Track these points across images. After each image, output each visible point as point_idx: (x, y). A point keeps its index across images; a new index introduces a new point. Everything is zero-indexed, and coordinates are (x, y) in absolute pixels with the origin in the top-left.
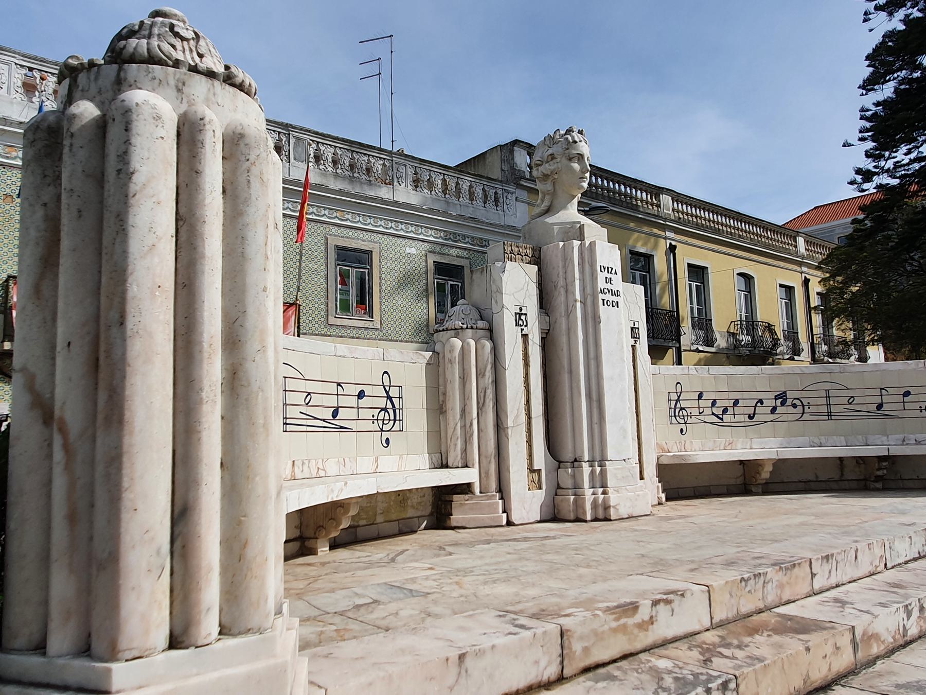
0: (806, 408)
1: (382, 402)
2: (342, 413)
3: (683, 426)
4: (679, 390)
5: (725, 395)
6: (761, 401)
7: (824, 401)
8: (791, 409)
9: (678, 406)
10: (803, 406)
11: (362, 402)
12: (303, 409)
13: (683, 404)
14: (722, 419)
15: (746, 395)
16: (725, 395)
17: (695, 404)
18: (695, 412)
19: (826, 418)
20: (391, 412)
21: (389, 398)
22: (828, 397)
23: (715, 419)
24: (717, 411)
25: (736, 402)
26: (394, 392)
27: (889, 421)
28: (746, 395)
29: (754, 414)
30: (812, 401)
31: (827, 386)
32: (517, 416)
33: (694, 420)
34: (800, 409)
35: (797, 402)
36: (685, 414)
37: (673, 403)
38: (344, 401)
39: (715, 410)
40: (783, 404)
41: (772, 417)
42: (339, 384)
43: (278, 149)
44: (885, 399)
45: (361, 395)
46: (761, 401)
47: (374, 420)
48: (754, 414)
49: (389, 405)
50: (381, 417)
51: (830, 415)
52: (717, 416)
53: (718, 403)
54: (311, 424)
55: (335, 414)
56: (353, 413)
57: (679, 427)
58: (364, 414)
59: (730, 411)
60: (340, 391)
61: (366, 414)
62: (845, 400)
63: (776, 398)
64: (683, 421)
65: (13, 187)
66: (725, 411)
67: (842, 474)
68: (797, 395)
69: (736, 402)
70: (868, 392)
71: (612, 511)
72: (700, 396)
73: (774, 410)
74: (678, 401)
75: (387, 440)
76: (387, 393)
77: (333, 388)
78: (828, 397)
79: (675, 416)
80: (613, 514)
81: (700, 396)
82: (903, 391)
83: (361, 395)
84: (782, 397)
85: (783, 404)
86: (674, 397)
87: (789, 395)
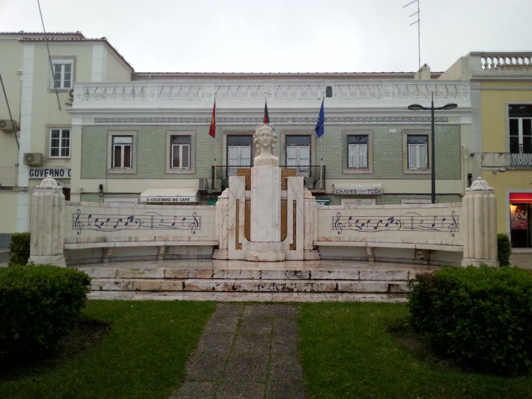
1: (452, 222)
2: (436, 226)
3: (340, 231)
5: (103, 217)
6: (381, 221)
7: (150, 221)
8: (395, 225)
9: (78, 221)
10: (401, 223)
11: (444, 222)
13: (80, 220)
15: (374, 218)
16: (103, 217)
18: (86, 224)
21: (454, 220)
25: (369, 221)
26: (456, 218)
27: (176, 230)
28: (374, 218)
30: (145, 221)
31: (412, 215)
32: (232, 226)
33: (85, 228)
34: (139, 224)
35: (398, 222)
37: (75, 219)
38: (176, 221)
39: (358, 224)
40: (391, 222)
41: (125, 227)
43: (414, 107)
45: (444, 220)
46: (381, 221)
47: (448, 228)
49: (195, 222)
51: (412, 228)
52: (358, 227)
54: (423, 228)
55: (433, 225)
56: (440, 226)
57: (77, 231)
59: (366, 225)
61: (446, 226)
62: (419, 222)
63: (128, 218)
66: (363, 225)
67: (213, 254)
68: (138, 217)
69: (369, 221)
70: (429, 218)
72: (90, 216)
73: (387, 225)
74: (338, 220)
75: (454, 235)
77: (433, 218)
81: (90, 216)
82: (443, 218)
83: (444, 220)
85: (391, 222)
86: (76, 216)
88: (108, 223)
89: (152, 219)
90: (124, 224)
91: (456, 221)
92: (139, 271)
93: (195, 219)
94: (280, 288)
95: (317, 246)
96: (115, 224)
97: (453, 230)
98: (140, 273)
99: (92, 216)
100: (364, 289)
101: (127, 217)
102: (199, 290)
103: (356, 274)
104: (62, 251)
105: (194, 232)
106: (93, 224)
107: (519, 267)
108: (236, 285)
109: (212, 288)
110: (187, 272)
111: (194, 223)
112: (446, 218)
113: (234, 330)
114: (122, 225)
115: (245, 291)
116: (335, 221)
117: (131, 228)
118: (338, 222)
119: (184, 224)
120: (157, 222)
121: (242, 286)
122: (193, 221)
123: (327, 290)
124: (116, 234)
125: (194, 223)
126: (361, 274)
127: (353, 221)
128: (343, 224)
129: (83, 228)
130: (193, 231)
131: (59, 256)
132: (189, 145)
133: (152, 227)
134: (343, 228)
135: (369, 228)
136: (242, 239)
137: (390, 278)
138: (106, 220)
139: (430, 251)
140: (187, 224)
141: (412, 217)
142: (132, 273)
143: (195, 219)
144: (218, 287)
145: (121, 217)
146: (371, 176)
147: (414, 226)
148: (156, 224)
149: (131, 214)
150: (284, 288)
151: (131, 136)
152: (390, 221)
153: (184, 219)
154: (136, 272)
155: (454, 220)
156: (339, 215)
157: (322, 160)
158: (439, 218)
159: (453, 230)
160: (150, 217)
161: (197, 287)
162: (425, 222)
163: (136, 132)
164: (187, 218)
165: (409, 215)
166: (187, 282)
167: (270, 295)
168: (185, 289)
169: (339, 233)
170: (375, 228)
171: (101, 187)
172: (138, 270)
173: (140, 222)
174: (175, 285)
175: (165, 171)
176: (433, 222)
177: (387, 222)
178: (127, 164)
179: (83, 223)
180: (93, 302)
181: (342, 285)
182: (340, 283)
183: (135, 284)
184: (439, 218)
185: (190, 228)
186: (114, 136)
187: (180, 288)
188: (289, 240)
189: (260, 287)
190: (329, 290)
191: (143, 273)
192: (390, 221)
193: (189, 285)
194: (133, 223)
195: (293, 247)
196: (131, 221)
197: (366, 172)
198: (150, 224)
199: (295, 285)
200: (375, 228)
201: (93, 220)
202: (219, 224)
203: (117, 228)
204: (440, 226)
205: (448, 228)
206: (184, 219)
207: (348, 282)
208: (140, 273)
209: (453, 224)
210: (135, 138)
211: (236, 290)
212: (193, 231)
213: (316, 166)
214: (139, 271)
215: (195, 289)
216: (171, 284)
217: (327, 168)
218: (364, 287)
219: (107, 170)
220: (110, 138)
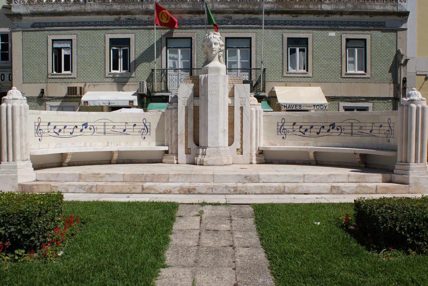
0: (343, 130)
1: (387, 128)
2: (373, 131)
3: (284, 136)
4: (39, 121)
6: (76, 127)
8: (336, 131)
9: (39, 128)
11: (381, 128)
13: (41, 127)
14: (58, 134)
17: (46, 127)
18: (46, 131)
19: (350, 135)
20: (146, 130)
21: (390, 127)
23: (301, 134)
24: (57, 131)
25: (65, 127)
26: (391, 125)
27: (128, 136)
29: (320, 132)
30: (98, 127)
31: (352, 121)
32: (182, 132)
33: (45, 134)
34: (93, 130)
35: (338, 127)
36: (42, 132)
38: (127, 127)
39: (301, 130)
40: (86, 128)
42: (373, 123)
44: (374, 128)
46: (76, 127)
47: (385, 134)
48: (320, 132)
49: (390, 129)
50: (387, 133)
52: (56, 133)
53: (57, 127)
55: (371, 131)
56: (378, 132)
57: (282, 136)
58: (381, 132)
59: (62, 131)
60: (373, 125)
61: (383, 132)
62: (358, 128)
63: (83, 125)
64: (40, 135)
65: (269, 32)
69: (65, 127)
71: (204, 162)
72: (49, 124)
73: (81, 130)
74: (39, 126)
76: (389, 125)
77: (371, 124)
78: (352, 126)
79: (280, 132)
80: (204, 163)
81: (49, 124)
82: (380, 124)
83: (381, 126)
84: (85, 125)
85: (333, 128)
86: (37, 124)
87: (336, 124)
88: (65, 130)
89: (105, 126)
90: (326, 131)
91: (392, 128)
92: (100, 176)
93: (145, 125)
94: (232, 190)
96: (71, 131)
97: (388, 136)
99: (51, 124)
100: (309, 191)
101: (82, 124)
102: (157, 192)
103: (301, 177)
104: (29, 158)
105: (144, 138)
108: (191, 188)
110: (144, 176)
111: (144, 129)
112: (383, 125)
113: (197, 227)
114: (77, 130)
115: (199, 193)
117: (86, 134)
118: (282, 128)
119: (135, 130)
120: (109, 128)
121: (197, 188)
122: (143, 127)
123: (275, 192)
125: (144, 129)
129: (43, 135)
130: (143, 136)
131: (27, 161)
132: (128, 48)
133: (105, 133)
137: (332, 180)
138: (63, 127)
140: (138, 130)
141: (352, 123)
142: (93, 177)
143: (145, 125)
144: (174, 190)
145: (76, 124)
146: (310, 79)
148: (109, 131)
149: (85, 121)
151: (71, 40)
152: (331, 127)
153: (135, 125)
154: (98, 176)
155: (390, 127)
156: (283, 121)
157: (262, 62)
159: (388, 136)
160: (103, 124)
161: (155, 190)
162: (116, 127)
163: (75, 36)
164: (137, 124)
166: (146, 185)
167: (223, 196)
168: (144, 191)
170: (71, 133)
171: (42, 92)
172: (99, 174)
173: (93, 129)
174: (134, 188)
176: (124, 128)
180: (69, 203)
181: (288, 188)
182: (286, 185)
183: (98, 187)
184: (376, 124)
185: (140, 134)
186: (53, 40)
187: (140, 190)
188: (237, 144)
190: (277, 192)
191: (104, 177)
192: (331, 127)
193: (147, 188)
194: (87, 130)
195: (241, 151)
196: (86, 128)
197: (306, 75)
198: (350, 131)
200: (71, 133)
202: (168, 130)
203: (74, 134)
204: (378, 132)
205: (385, 134)
206: (135, 125)
207: (294, 185)
209: (389, 131)
210: (74, 42)
211: (191, 193)
212: (143, 136)
215: (153, 192)
216: (131, 187)
219: (48, 75)
220: (50, 42)
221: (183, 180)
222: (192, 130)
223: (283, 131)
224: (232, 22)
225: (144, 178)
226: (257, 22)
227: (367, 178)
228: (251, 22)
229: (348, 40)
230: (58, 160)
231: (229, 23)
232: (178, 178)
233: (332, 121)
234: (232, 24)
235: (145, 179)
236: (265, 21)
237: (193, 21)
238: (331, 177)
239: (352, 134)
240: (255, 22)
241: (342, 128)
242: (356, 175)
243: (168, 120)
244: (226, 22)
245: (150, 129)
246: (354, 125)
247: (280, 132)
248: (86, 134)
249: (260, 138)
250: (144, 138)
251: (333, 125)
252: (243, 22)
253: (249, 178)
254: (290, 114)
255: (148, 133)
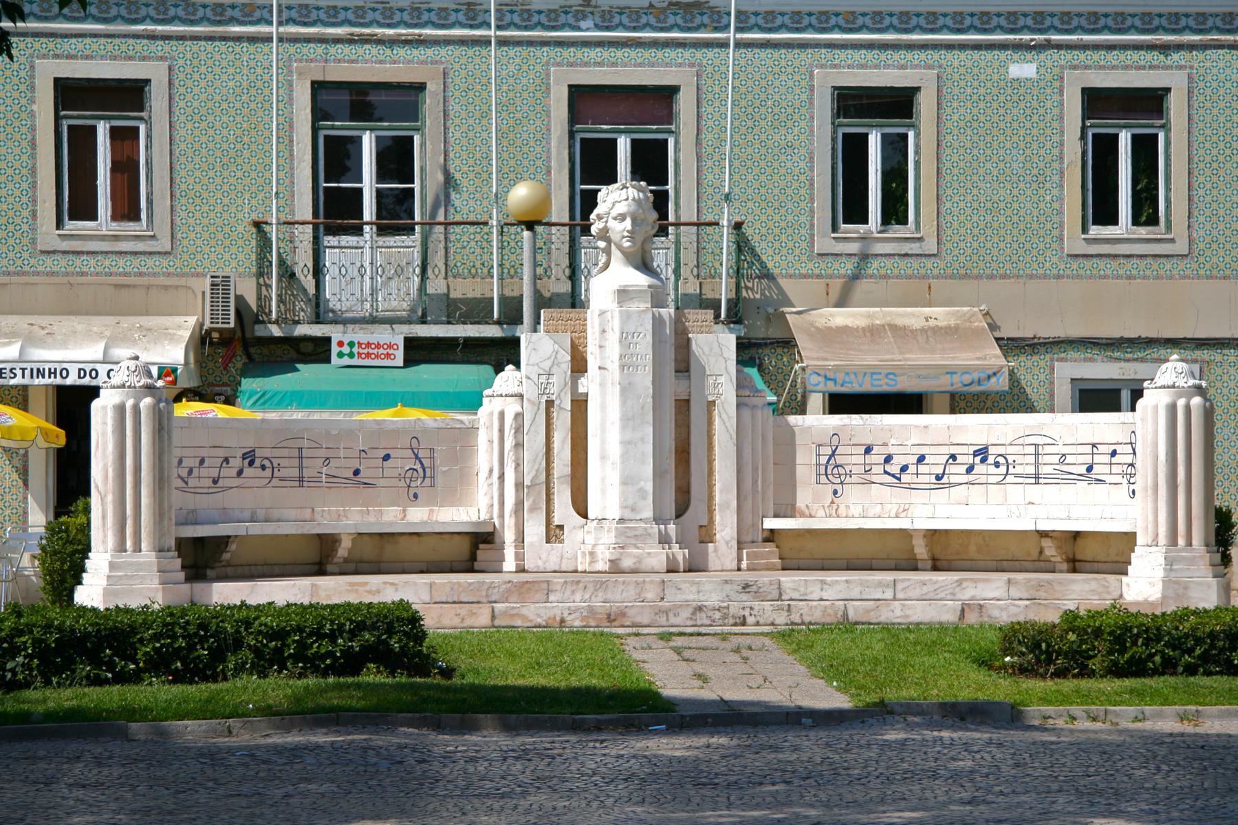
2: (1096, 469)
3: (839, 488)
6: (953, 457)
7: (1032, 459)
8: (992, 469)
11: (1114, 460)
12: (1057, 467)
13: (839, 460)
14: (899, 479)
17: (860, 459)
19: (1033, 481)
20: (420, 471)
21: (417, 457)
22: (301, 458)
23: (889, 479)
24: (895, 469)
25: (921, 459)
29: (944, 474)
30: (1019, 459)
33: (855, 479)
34: (268, 472)
35: (1001, 460)
38: (1097, 459)
39: (888, 468)
41: (965, 479)
42: (1094, 445)
45: (1114, 453)
47: (1123, 474)
48: (944, 474)
49: (418, 466)
51: (1037, 477)
52: (893, 476)
53: (895, 460)
54: (1064, 477)
55: (1090, 469)
56: (1106, 469)
58: (1115, 469)
59: (912, 469)
60: (1095, 450)
63: (975, 454)
66: (190, 472)
68: (1001, 450)
72: (868, 450)
73: (970, 470)
77: (1088, 449)
79: (826, 474)
81: (868, 450)
83: (1114, 453)
84: (982, 453)
87: (992, 450)
88: (922, 468)
90: (963, 469)
92: (368, 588)
95: (772, 531)
98: (370, 592)
100: (907, 616)
101: (972, 449)
103: (888, 586)
106: (878, 469)
107: (248, 602)
109: (558, 619)
110: (486, 587)
112: (1119, 449)
116: (824, 460)
117: (250, 482)
121: (631, 612)
124: (217, 500)
126: (900, 586)
127: (876, 458)
128: (848, 468)
134: (848, 480)
135: (922, 479)
136: (563, 510)
139: (1076, 535)
145: (953, 450)
147: (1044, 470)
149: (982, 440)
150: (725, 617)
154: (361, 589)
156: (835, 442)
158: (1102, 448)
160: (1032, 449)
162: (1069, 459)
165: (290, 443)
169: (835, 492)
170: (939, 478)
175: (34, 241)
176: (1088, 459)
177: (970, 459)
178: (127, 208)
179: (848, 468)
185: (402, 483)
189: (671, 615)
191: (378, 592)
192: (978, 459)
199: (751, 608)
200: (939, 478)
201: (876, 458)
202: (491, 471)
203: (945, 480)
208: (370, 592)
213: (698, 225)
214: (368, 588)
217: (747, 230)
218: (908, 612)
221: (587, 596)
222: (568, 470)
223: (835, 471)
224: (598, 21)
225: (484, 593)
226: (706, 19)
227: (1057, 587)
228: (680, 21)
229: (577, 93)
230: (312, 554)
231: (583, 24)
232: (573, 592)
233: (250, 443)
234: (598, 27)
235: (487, 596)
236: (739, 13)
237: (430, 10)
238: (965, 584)
239: (1037, 477)
240: (698, 20)
241: (1010, 461)
242: (1029, 580)
243: (491, 442)
244: (571, 20)
245: (432, 468)
246: (305, 453)
247: (826, 474)
248: (250, 482)
249: (764, 492)
250: (416, 496)
251: (250, 457)
252: (644, 20)
253: (754, 588)
254: (854, 422)
255: (428, 481)
